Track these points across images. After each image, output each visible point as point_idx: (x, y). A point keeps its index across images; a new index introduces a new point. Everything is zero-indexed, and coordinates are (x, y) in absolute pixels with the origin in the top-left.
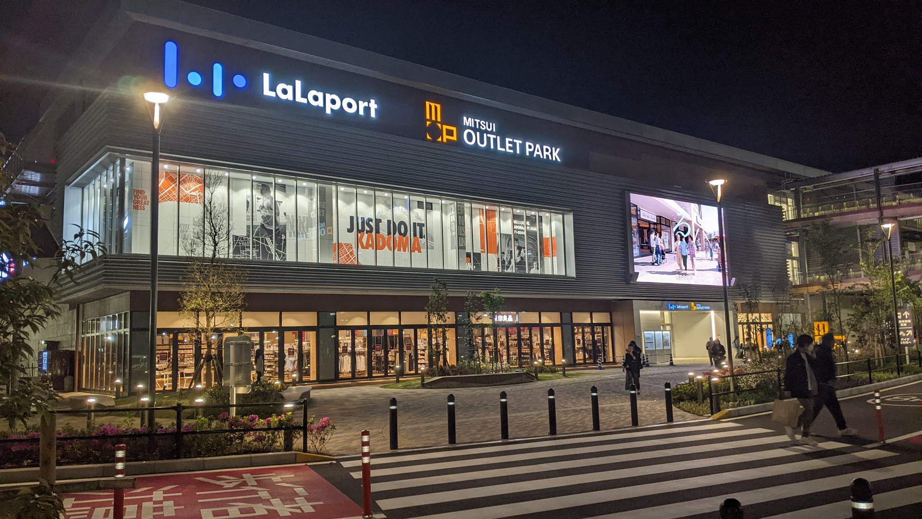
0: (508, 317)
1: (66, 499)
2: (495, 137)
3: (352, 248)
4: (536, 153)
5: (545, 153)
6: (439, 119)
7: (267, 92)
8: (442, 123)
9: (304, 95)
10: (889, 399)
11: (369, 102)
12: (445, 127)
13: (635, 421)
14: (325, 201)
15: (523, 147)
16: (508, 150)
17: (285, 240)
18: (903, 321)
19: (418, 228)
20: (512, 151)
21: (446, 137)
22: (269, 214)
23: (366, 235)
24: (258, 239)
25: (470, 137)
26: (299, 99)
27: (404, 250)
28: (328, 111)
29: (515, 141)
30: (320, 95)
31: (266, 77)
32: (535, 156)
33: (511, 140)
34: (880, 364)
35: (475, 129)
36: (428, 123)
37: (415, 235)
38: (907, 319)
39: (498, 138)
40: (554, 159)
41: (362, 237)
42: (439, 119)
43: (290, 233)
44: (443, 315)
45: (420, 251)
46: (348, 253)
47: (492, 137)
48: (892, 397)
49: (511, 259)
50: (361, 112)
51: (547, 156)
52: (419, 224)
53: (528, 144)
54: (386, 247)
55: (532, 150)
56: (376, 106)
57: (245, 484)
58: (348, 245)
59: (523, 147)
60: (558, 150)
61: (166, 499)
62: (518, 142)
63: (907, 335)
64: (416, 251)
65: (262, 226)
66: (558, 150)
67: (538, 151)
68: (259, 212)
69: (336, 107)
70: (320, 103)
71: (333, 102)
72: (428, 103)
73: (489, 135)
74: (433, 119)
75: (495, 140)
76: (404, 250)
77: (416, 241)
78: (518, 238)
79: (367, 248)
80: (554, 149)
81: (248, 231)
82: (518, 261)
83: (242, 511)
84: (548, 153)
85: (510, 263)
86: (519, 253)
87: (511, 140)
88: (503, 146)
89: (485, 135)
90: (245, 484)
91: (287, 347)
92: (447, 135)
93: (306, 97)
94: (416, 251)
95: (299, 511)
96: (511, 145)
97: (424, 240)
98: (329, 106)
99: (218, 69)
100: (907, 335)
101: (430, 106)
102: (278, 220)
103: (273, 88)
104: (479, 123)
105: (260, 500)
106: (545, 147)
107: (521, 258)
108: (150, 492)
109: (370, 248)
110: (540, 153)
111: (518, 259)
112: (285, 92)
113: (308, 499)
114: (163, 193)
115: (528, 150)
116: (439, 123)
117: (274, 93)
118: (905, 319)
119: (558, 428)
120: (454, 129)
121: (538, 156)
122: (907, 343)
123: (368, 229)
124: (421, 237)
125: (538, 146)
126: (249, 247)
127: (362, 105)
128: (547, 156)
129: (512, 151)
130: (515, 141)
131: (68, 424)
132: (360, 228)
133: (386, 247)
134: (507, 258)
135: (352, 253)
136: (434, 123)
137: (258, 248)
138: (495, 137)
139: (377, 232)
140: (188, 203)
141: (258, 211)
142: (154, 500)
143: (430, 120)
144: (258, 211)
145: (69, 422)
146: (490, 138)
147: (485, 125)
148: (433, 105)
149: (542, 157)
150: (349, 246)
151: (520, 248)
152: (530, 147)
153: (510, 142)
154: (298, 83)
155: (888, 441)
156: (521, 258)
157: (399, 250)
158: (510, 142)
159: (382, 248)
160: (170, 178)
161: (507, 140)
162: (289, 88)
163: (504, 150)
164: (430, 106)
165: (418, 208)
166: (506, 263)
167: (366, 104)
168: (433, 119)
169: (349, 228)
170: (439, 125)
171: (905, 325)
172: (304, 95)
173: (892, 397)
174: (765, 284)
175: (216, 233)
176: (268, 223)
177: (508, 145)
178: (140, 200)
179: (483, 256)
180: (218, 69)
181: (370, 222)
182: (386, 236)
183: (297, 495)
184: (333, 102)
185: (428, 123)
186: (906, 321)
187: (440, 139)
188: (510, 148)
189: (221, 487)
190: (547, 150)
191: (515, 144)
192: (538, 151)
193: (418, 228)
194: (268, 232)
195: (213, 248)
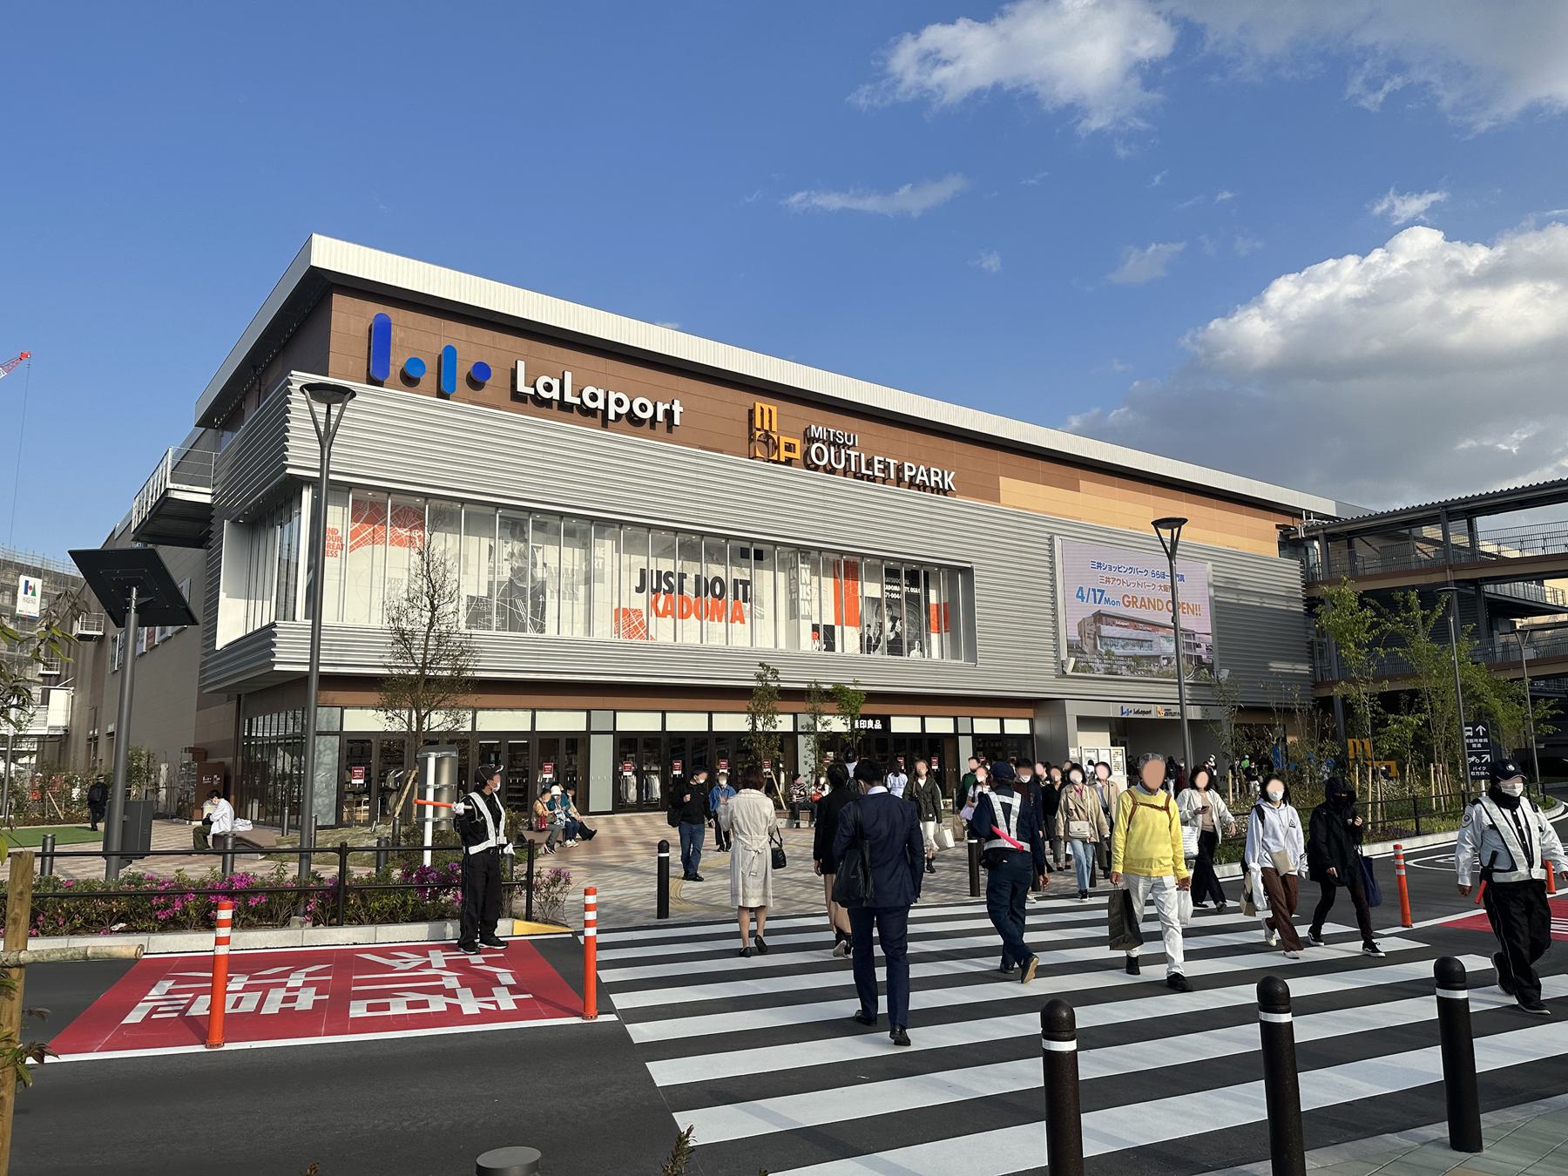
0: (874, 723)
1: (1023, 939)
3: (642, 616)
4: (919, 477)
6: (774, 429)
8: (781, 432)
10: (1441, 861)
13: (663, 910)
14: (604, 547)
17: (544, 603)
18: (1476, 740)
19: (740, 586)
22: (521, 565)
23: (662, 597)
24: (505, 602)
27: (721, 621)
29: (887, 460)
34: (1439, 808)
37: (736, 597)
38: (1482, 737)
41: (657, 599)
43: (552, 592)
44: (773, 717)
45: (743, 622)
46: (636, 623)
48: (1446, 857)
49: (880, 634)
52: (742, 582)
54: (693, 615)
55: (913, 473)
57: (428, 965)
58: (636, 610)
60: (953, 474)
61: (306, 984)
63: (1483, 761)
64: (738, 622)
65: (511, 581)
67: (922, 475)
68: (508, 562)
71: (619, 402)
73: (848, 452)
74: (766, 427)
76: (720, 620)
77: (738, 607)
78: (892, 604)
79: (664, 615)
81: (490, 590)
82: (892, 637)
83: (410, 1005)
84: (938, 479)
85: (878, 640)
86: (893, 627)
90: (428, 965)
91: (272, 788)
94: (738, 622)
95: (493, 1007)
96: (882, 467)
97: (748, 605)
100: (1483, 761)
102: (535, 575)
105: (441, 990)
106: (932, 470)
107: (896, 633)
108: (286, 974)
109: (669, 616)
110: (925, 478)
111: (892, 636)
113: (513, 990)
114: (366, 533)
117: (533, 389)
118: (1480, 737)
119: (672, 905)
122: (1483, 773)
123: (667, 588)
124: (745, 600)
126: (490, 613)
128: (936, 482)
131: (178, 871)
132: (655, 587)
133: (693, 615)
134: (874, 634)
135: (641, 624)
137: (504, 614)
138: (857, 454)
139: (681, 592)
140: (402, 548)
141: (505, 560)
142: (288, 986)
144: (505, 560)
145: (181, 867)
146: (849, 455)
147: (844, 436)
150: (638, 612)
151: (894, 619)
152: (911, 469)
155: (1416, 926)
156: (896, 633)
157: (712, 620)
158: (880, 462)
159: (688, 616)
165: (742, 557)
166: (873, 641)
168: (766, 427)
169: (638, 586)
171: (1479, 746)
173: (1446, 857)
175: (434, 591)
176: (519, 579)
178: (331, 542)
179: (838, 629)
181: (670, 579)
182: (693, 600)
183: (499, 984)
184: (619, 402)
186: (1481, 740)
189: (390, 969)
192: (922, 475)
193: (740, 586)
194: (519, 592)
195: (430, 614)
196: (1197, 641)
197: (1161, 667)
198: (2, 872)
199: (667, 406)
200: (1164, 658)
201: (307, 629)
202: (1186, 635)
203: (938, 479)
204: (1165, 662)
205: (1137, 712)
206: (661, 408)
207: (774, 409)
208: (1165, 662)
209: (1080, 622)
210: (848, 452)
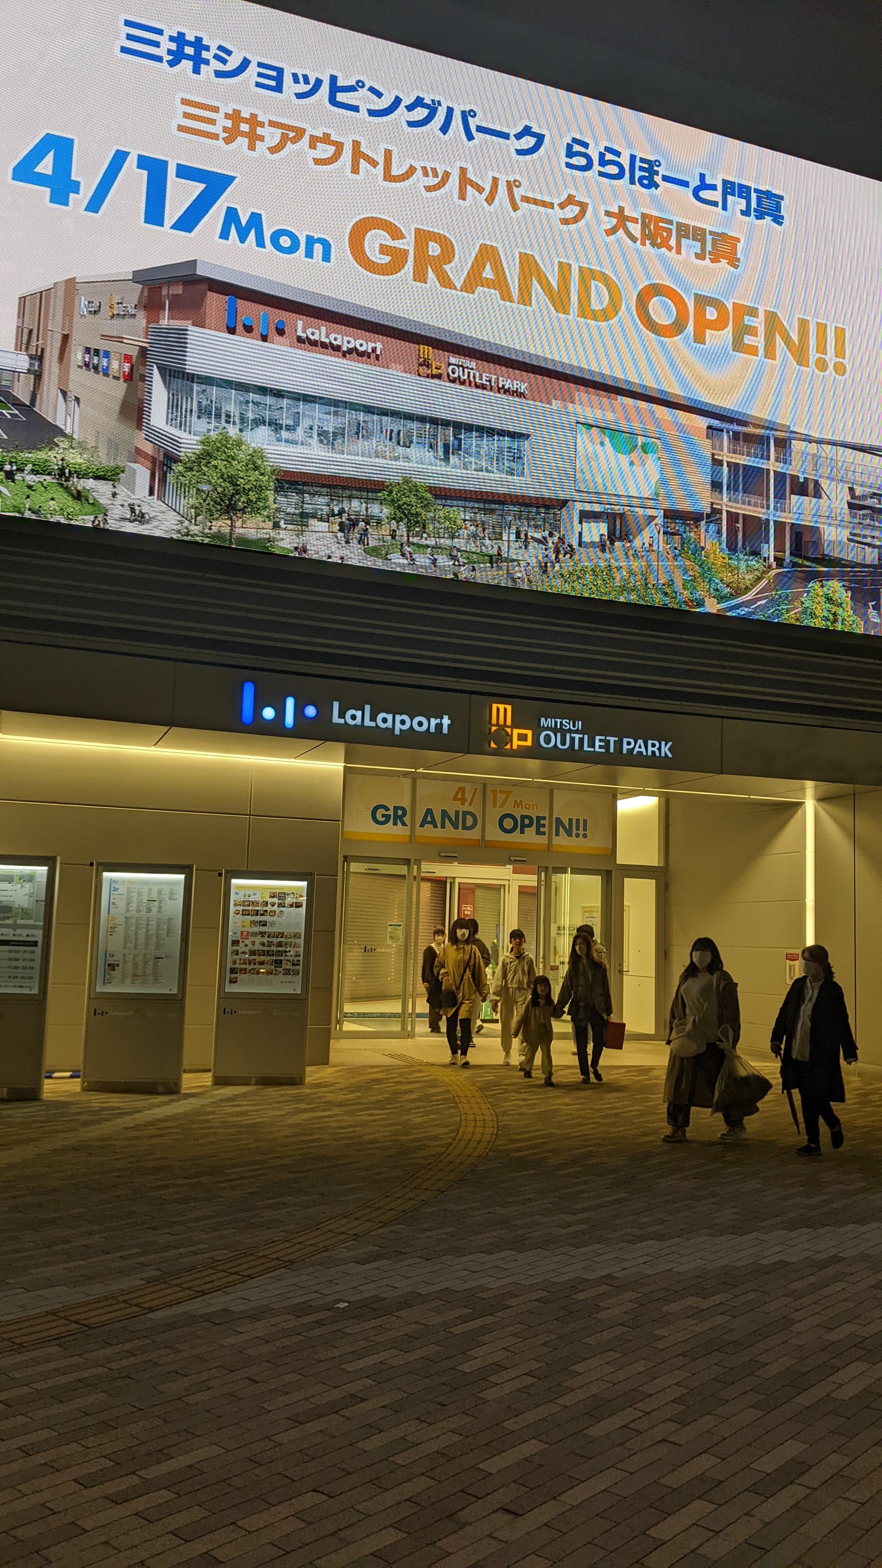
2: (581, 736)
4: (637, 749)
5: (650, 749)
7: (336, 719)
8: (513, 726)
9: (373, 718)
11: (442, 718)
12: (516, 732)
15: (618, 744)
16: (597, 749)
20: (603, 750)
21: (516, 743)
25: (548, 739)
26: (368, 723)
28: (397, 732)
29: (608, 738)
30: (389, 717)
31: (336, 705)
32: (635, 753)
33: (603, 738)
35: (555, 730)
36: (494, 728)
39: (586, 737)
40: (663, 754)
42: (509, 722)
47: (577, 736)
50: (432, 730)
51: (653, 752)
53: (625, 740)
56: (449, 722)
59: (618, 744)
60: (670, 744)
62: (612, 740)
66: (670, 744)
67: (640, 747)
69: (407, 726)
70: (389, 724)
72: (494, 706)
73: (573, 735)
75: (581, 740)
80: (663, 743)
87: (603, 738)
88: (592, 744)
89: (568, 735)
92: (519, 740)
93: (375, 720)
96: (603, 744)
98: (398, 726)
99: (290, 703)
101: (498, 709)
103: (342, 715)
104: (561, 723)
110: (643, 750)
112: (385, 720)
115: (625, 747)
116: (509, 727)
120: (529, 733)
121: (640, 753)
125: (640, 742)
127: (434, 722)
129: (603, 750)
130: (608, 738)
136: (502, 728)
138: (581, 736)
143: (497, 724)
146: (574, 738)
148: (501, 707)
149: (645, 753)
153: (600, 741)
154: (367, 708)
158: (600, 741)
160: (462, 790)
161: (598, 738)
162: (359, 714)
163: (342, 721)
164: (498, 709)
167: (438, 721)
168: (501, 722)
170: (509, 730)
172: (373, 718)
174: (187, 403)
177: (597, 743)
180: (290, 703)
185: (494, 728)
187: (508, 747)
188: (600, 747)
190: (653, 745)
191: (608, 743)
192: (640, 747)
196: (796, 468)
197: (564, 549)
198: (880, 1121)
199: (438, 721)
200: (585, 516)
201: (352, 1015)
202: (736, 436)
203: (655, 749)
204: (596, 531)
205: (18, 952)
206: (434, 722)
207: (509, 708)
208: (596, 531)
209: (43, 296)
210: (573, 735)
